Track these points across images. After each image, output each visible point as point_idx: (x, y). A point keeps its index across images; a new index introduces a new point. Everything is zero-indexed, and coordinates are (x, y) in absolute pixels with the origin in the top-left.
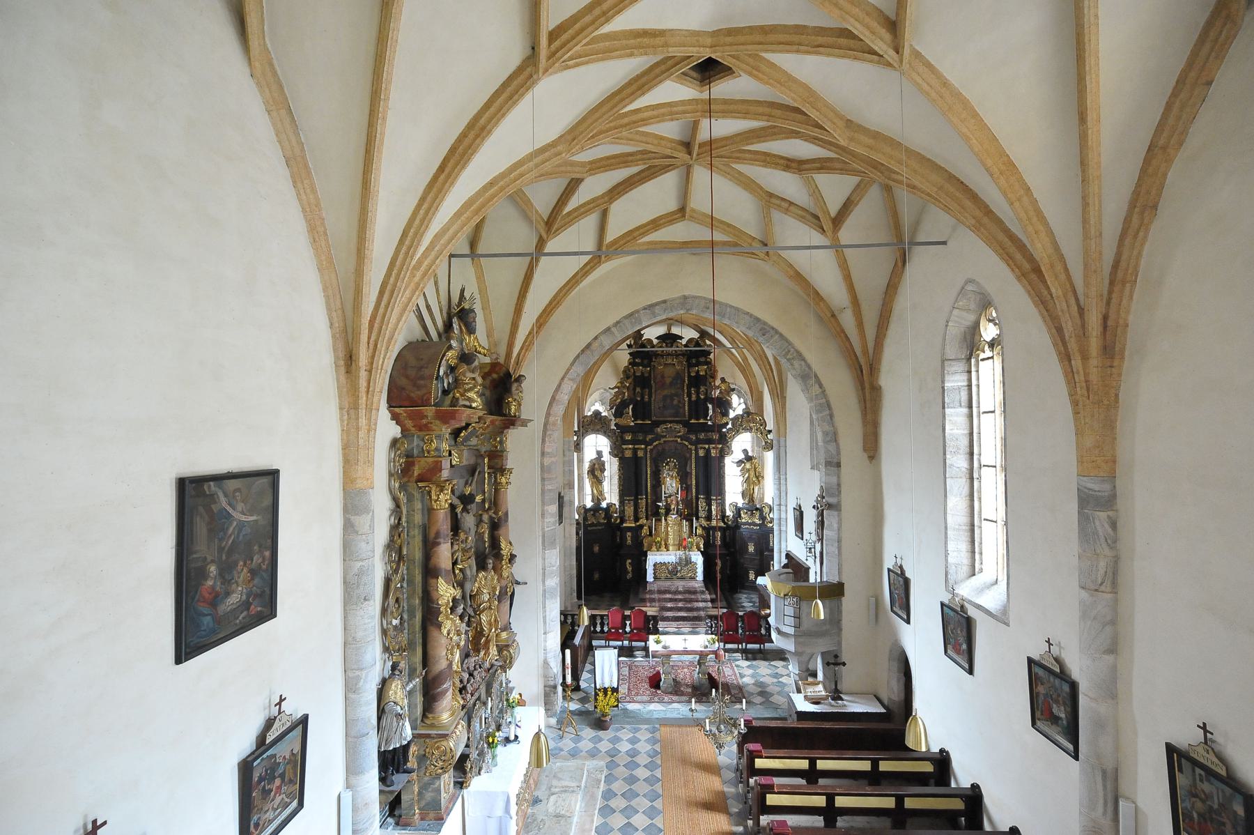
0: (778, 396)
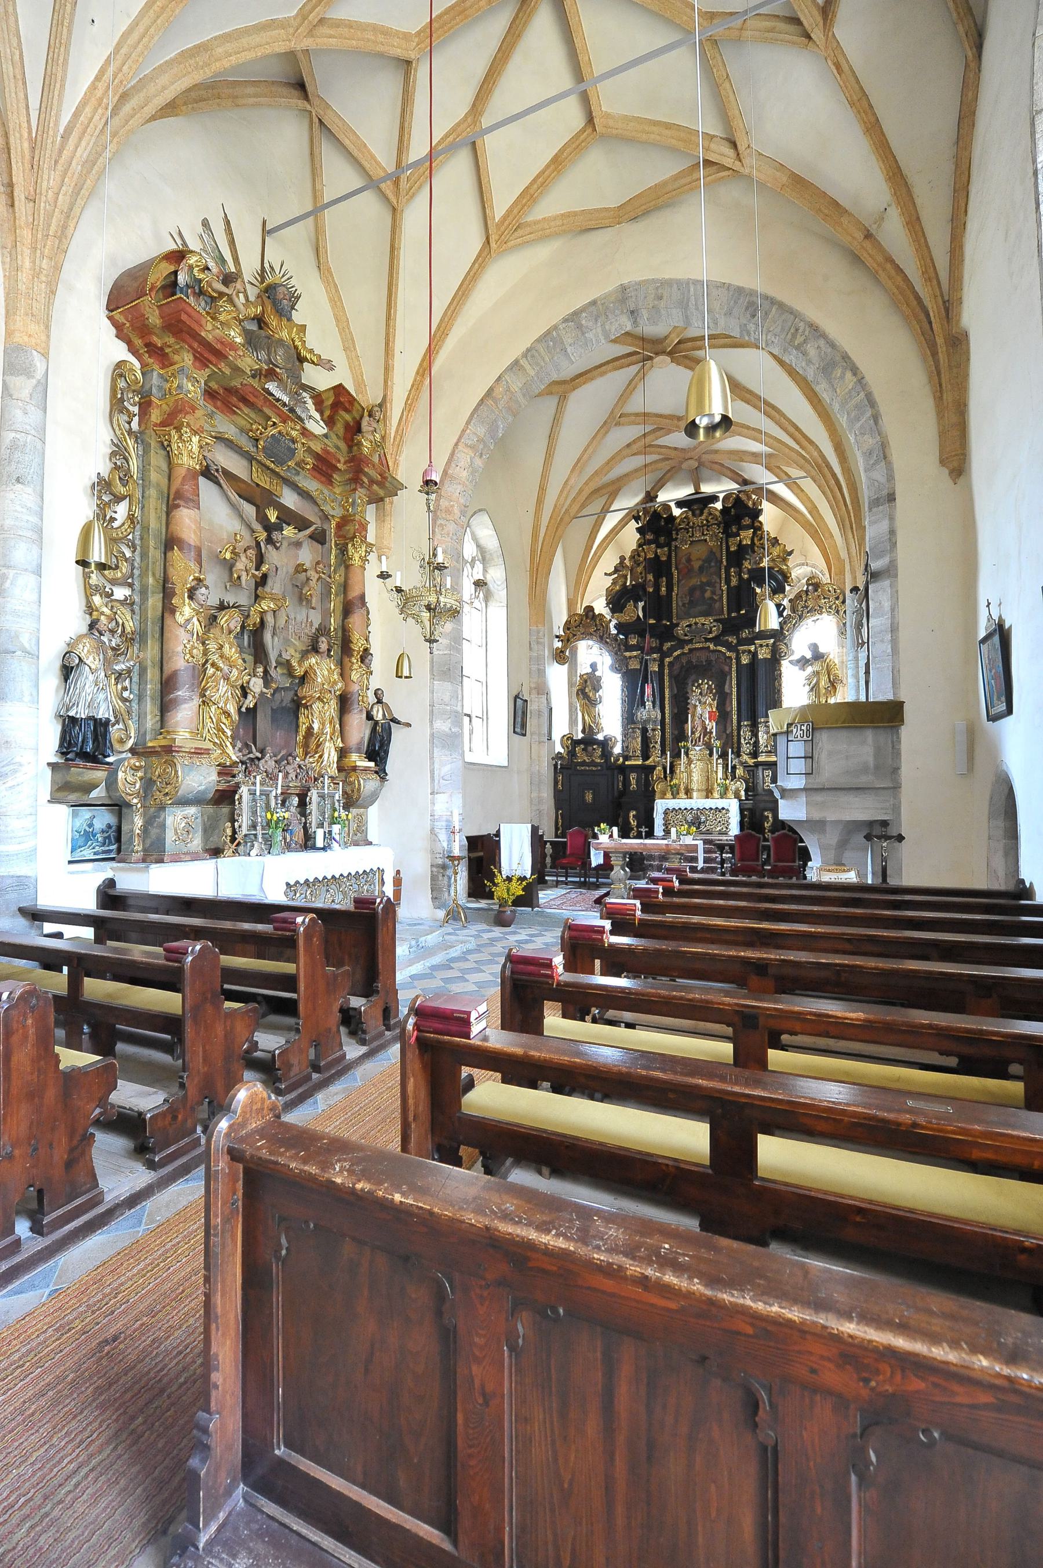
0: (852, 528)
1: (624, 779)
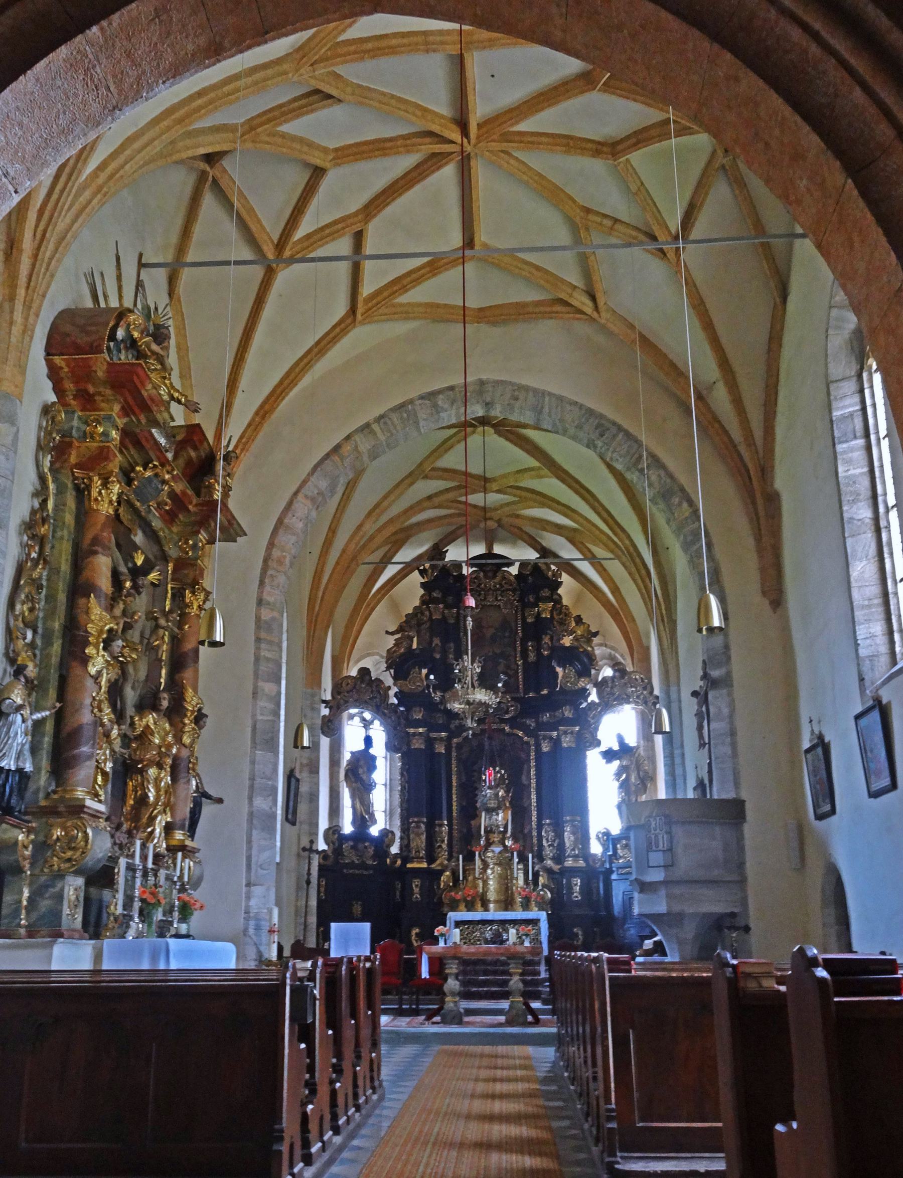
1: (403, 888)
